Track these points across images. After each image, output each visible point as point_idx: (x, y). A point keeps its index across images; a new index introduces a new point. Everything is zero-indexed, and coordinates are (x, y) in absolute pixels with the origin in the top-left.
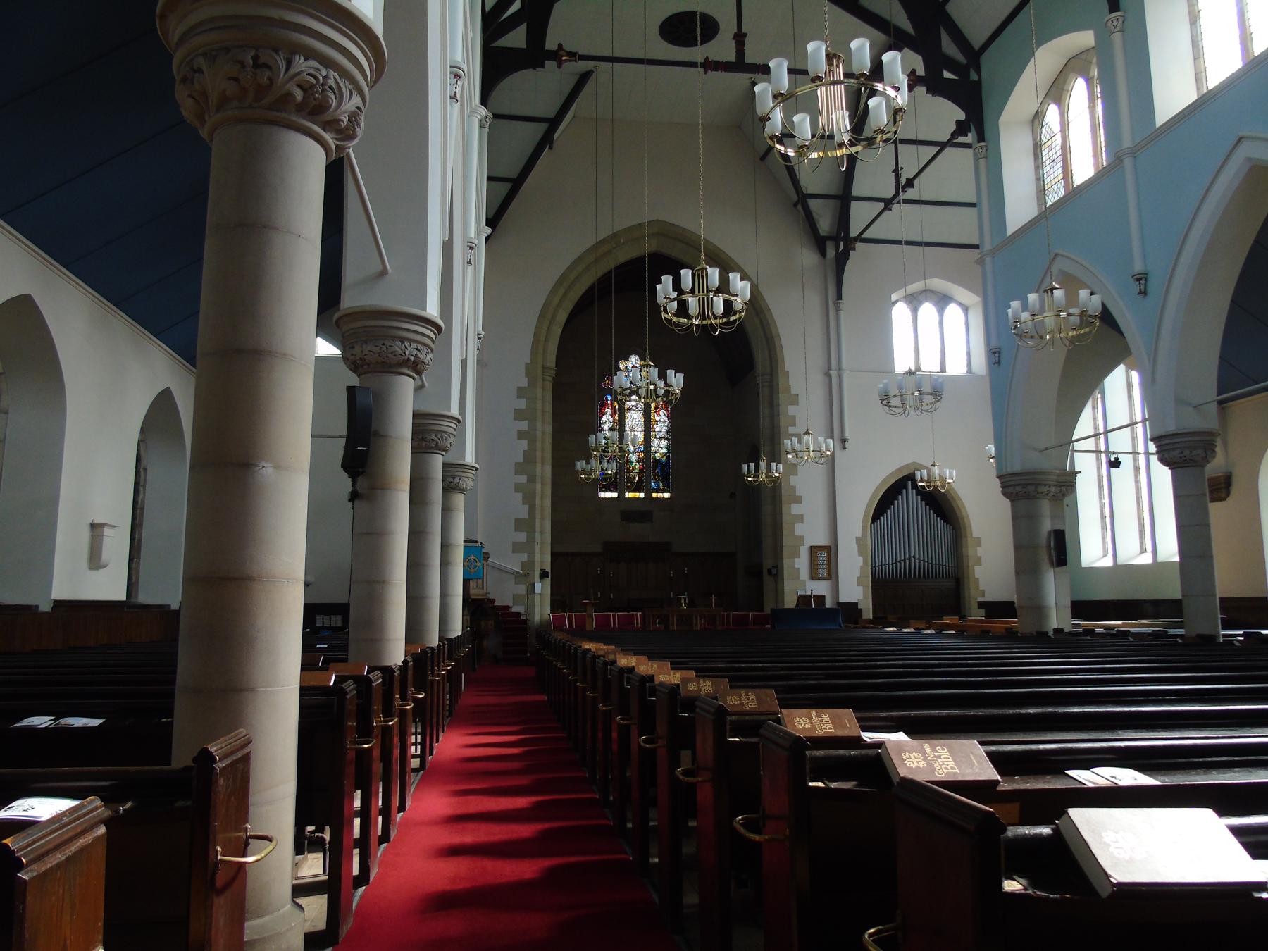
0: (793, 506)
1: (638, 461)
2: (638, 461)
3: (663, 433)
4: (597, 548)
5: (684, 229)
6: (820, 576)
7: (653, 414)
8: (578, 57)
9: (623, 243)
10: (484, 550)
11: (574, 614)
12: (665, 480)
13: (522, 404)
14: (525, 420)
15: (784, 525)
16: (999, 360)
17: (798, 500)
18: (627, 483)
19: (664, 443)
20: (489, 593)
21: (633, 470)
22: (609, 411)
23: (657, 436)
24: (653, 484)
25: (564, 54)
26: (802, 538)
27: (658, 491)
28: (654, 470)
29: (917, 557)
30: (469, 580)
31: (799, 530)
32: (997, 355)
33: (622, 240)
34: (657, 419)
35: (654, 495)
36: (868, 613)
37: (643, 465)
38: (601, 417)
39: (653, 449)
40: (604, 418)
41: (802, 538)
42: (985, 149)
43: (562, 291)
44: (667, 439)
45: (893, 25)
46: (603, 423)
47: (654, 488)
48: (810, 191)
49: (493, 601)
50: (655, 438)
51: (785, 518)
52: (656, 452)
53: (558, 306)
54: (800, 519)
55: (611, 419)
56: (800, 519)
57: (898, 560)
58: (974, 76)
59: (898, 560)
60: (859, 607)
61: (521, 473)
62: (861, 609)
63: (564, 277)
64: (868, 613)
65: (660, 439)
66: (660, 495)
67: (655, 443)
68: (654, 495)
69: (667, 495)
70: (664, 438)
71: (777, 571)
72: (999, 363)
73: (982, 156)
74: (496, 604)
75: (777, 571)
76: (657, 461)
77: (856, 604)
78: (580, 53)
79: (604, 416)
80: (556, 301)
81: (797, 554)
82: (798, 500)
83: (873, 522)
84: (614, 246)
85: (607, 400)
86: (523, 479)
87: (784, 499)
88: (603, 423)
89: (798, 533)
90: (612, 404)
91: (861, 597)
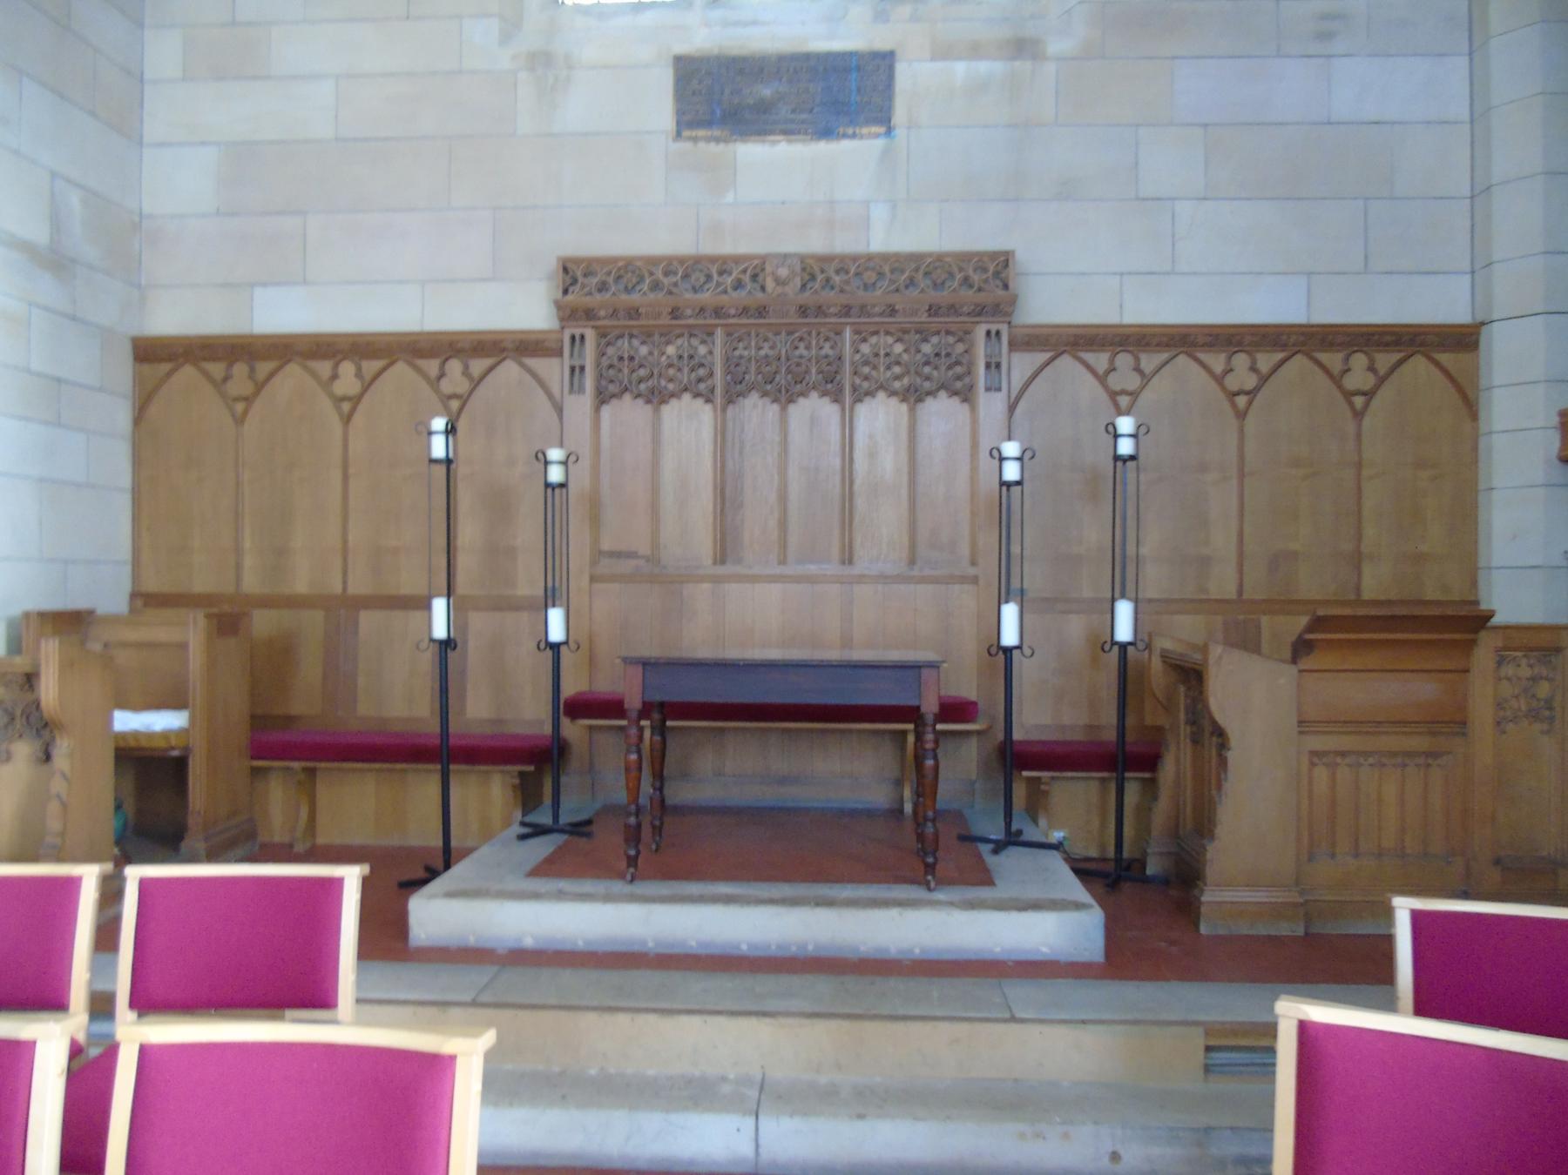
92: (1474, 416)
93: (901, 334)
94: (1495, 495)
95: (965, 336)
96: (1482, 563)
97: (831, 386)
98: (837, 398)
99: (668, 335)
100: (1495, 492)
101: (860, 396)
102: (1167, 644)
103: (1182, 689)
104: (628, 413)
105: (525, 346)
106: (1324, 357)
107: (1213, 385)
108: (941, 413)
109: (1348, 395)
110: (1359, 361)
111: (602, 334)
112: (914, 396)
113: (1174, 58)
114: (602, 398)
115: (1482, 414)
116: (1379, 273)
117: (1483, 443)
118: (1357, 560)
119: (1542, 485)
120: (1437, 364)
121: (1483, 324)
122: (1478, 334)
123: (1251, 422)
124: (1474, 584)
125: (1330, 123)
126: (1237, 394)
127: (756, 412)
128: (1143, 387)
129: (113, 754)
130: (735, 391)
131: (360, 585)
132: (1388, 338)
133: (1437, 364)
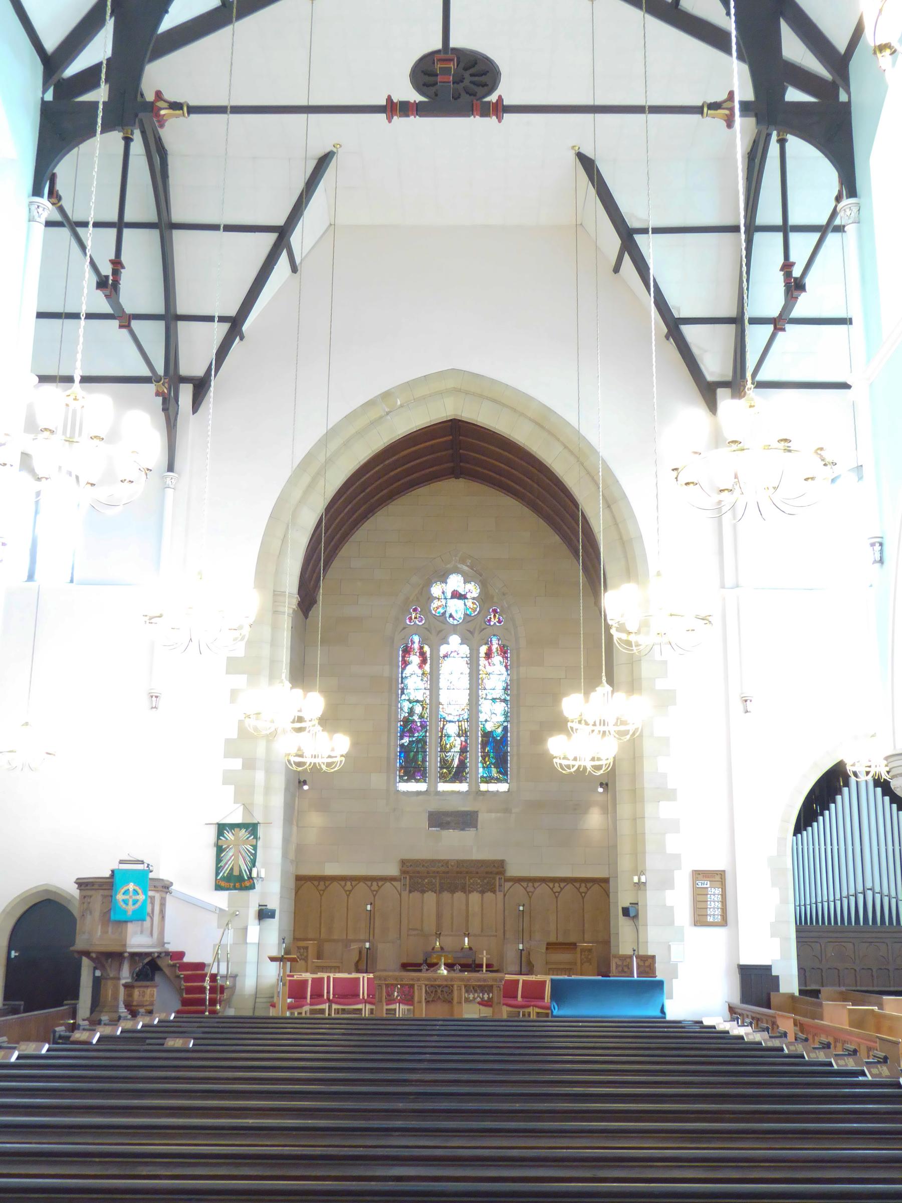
0: (663, 804)
1: (459, 736)
2: (459, 736)
3: (499, 693)
4: (393, 870)
5: (493, 381)
6: (710, 919)
7: (483, 661)
8: (185, 109)
9: (401, 406)
10: (151, 875)
11: (332, 975)
12: (501, 762)
13: (240, 651)
14: (244, 673)
15: (647, 837)
16: (881, 558)
17: (670, 795)
18: (442, 768)
19: (500, 707)
20: (169, 943)
21: (451, 748)
22: (415, 659)
23: (490, 697)
24: (481, 770)
25: (166, 105)
26: (677, 857)
27: (488, 780)
28: (483, 747)
29: (877, 889)
30: (126, 922)
31: (672, 844)
32: (877, 547)
33: (399, 403)
34: (489, 669)
35: (484, 787)
36: (790, 984)
37: (466, 741)
38: (404, 669)
39: (482, 717)
40: (409, 670)
41: (677, 857)
42: (855, 210)
43: (306, 479)
44: (505, 701)
45: (640, 8)
46: (406, 677)
47: (482, 777)
48: (684, 314)
49: (181, 955)
50: (485, 699)
51: (650, 826)
52: (486, 721)
53: (302, 500)
54: (674, 826)
55: (420, 672)
56: (674, 826)
57: (845, 894)
58: (843, 97)
59: (845, 894)
60: (774, 973)
61: (235, 756)
62: (777, 977)
63: (309, 457)
64: (790, 984)
65: (494, 700)
66: (493, 787)
67: (485, 707)
68: (484, 787)
69: (503, 787)
70: (500, 699)
71: (94, 973)
72: (881, 561)
73: (850, 221)
74: (186, 960)
75: (94, 973)
76: (487, 735)
77: (768, 968)
78: (192, 103)
79: (408, 667)
80: (298, 493)
81: (668, 883)
82: (670, 795)
83: (798, 830)
84: (387, 410)
85: (413, 643)
86: (236, 764)
87: (648, 794)
88: (406, 677)
89: (670, 849)
90: (421, 648)
91: (777, 957)
93: (479, 878)
95: (494, 879)
97: (464, 890)
98: (465, 892)
99: (426, 877)
101: (470, 892)
104: (416, 895)
105: (392, 879)
108: (489, 896)
110: (583, 885)
111: (411, 878)
112: (482, 892)
114: (410, 892)
127: (446, 895)
130: (442, 890)
131: (351, 937)
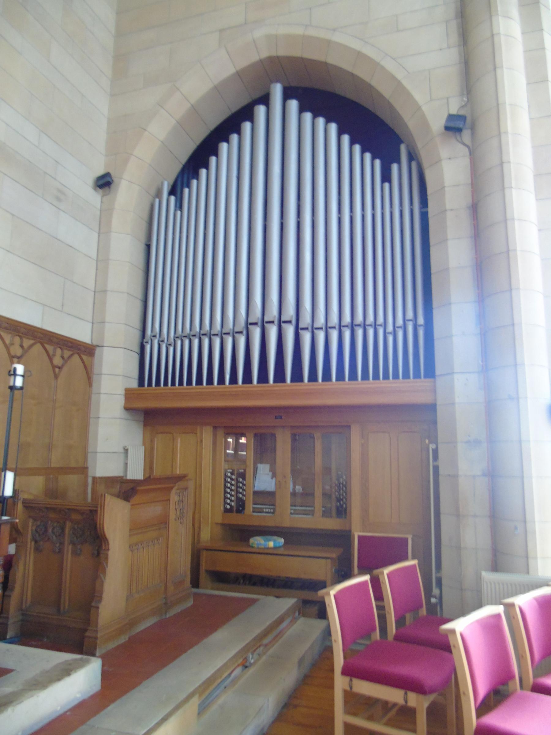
92: (90, 385)
94: (101, 421)
96: (90, 449)
100: (100, 419)
102: (26, 496)
103: (31, 521)
106: (47, 346)
107: (4, 350)
109: (54, 367)
113: (5, 174)
115: (94, 385)
116: (66, 313)
117: (94, 398)
118: (50, 447)
119: (119, 418)
120: (45, 349)
121: (98, 346)
122: (95, 350)
123: (61, 380)
124: (86, 459)
125: (56, 238)
126: (14, 357)
128: (9, 353)
129: (384, 599)
132: (70, 344)
133: (45, 349)
